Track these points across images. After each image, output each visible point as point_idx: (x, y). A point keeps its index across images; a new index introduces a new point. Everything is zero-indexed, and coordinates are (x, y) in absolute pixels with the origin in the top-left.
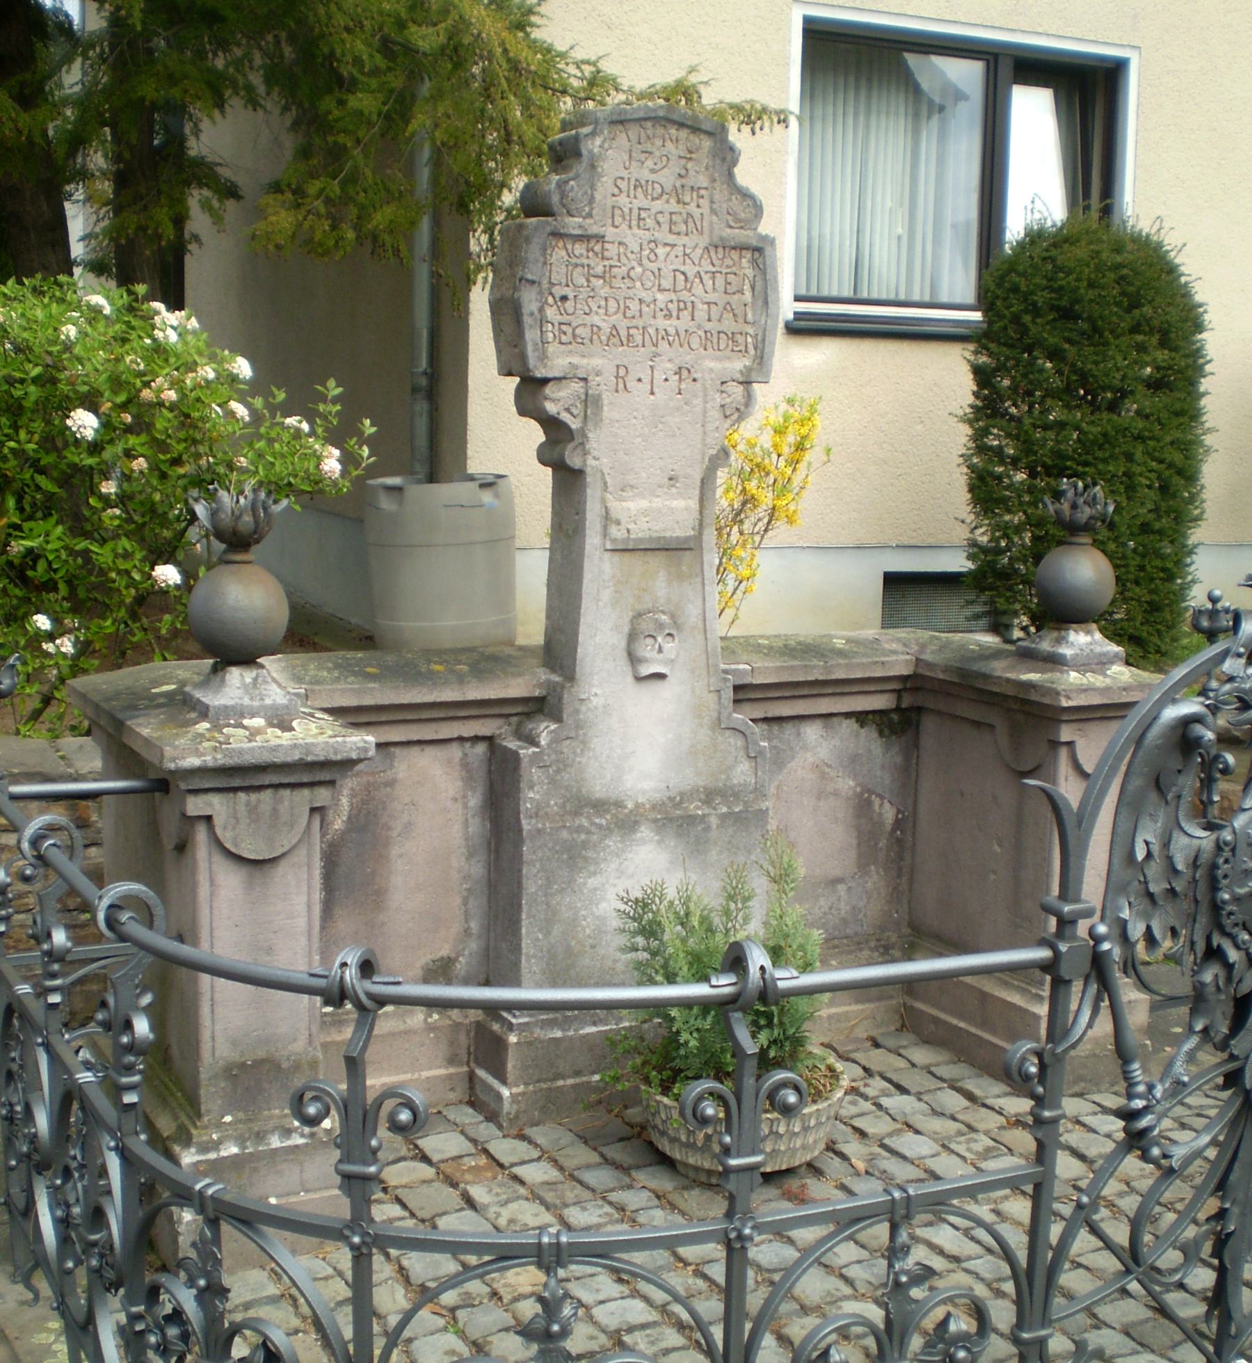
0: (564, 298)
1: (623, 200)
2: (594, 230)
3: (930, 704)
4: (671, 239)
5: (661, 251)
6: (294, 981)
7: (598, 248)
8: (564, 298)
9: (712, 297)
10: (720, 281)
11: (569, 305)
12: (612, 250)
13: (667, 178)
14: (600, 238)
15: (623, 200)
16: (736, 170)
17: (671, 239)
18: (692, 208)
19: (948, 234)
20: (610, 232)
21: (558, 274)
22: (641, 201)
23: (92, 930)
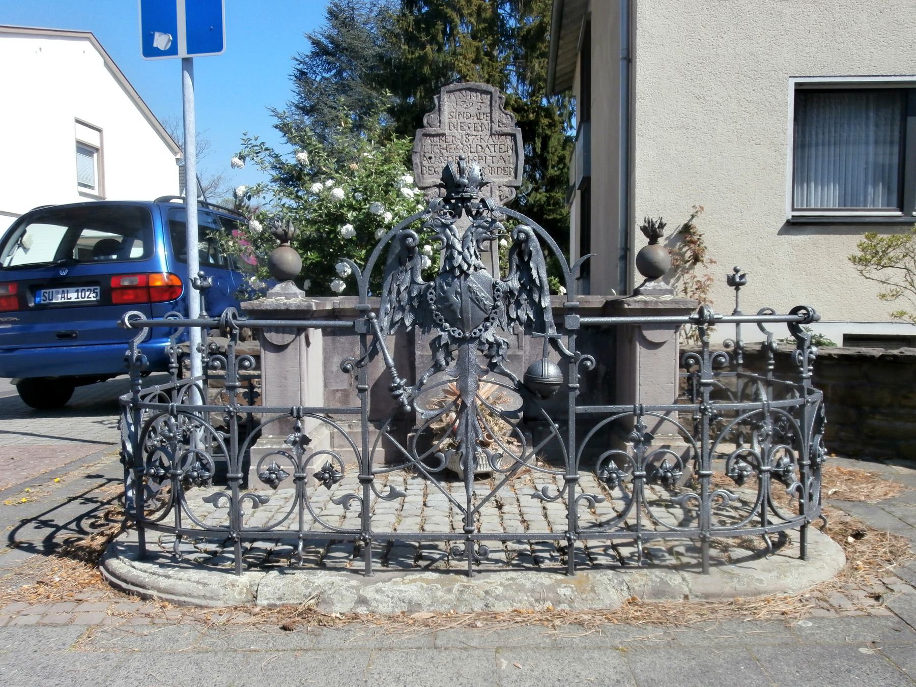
0: (430, 158)
1: (454, 120)
2: (441, 132)
3: (123, 431)
4: (474, 133)
5: (470, 138)
6: (898, 188)
7: (444, 138)
8: (430, 158)
9: (494, 154)
10: (497, 147)
11: (433, 160)
12: (450, 139)
13: (473, 110)
14: (443, 135)
15: (454, 120)
16: (86, 45)
17: (474, 133)
18: (484, 121)
19: (437, 108)
20: (447, 132)
21: (428, 148)
22: (462, 120)
23: (849, 203)
